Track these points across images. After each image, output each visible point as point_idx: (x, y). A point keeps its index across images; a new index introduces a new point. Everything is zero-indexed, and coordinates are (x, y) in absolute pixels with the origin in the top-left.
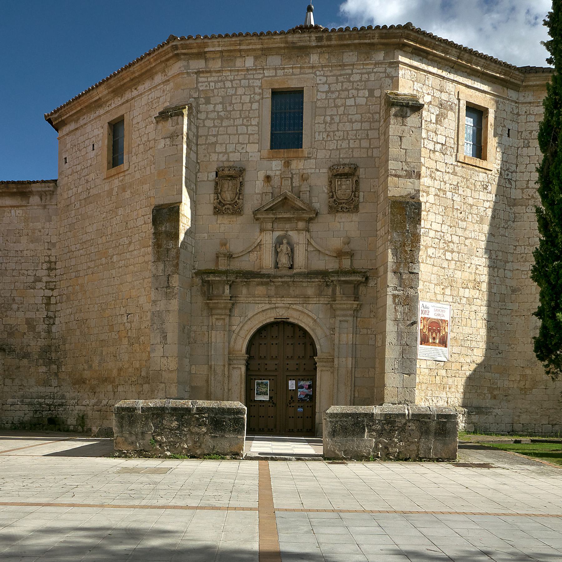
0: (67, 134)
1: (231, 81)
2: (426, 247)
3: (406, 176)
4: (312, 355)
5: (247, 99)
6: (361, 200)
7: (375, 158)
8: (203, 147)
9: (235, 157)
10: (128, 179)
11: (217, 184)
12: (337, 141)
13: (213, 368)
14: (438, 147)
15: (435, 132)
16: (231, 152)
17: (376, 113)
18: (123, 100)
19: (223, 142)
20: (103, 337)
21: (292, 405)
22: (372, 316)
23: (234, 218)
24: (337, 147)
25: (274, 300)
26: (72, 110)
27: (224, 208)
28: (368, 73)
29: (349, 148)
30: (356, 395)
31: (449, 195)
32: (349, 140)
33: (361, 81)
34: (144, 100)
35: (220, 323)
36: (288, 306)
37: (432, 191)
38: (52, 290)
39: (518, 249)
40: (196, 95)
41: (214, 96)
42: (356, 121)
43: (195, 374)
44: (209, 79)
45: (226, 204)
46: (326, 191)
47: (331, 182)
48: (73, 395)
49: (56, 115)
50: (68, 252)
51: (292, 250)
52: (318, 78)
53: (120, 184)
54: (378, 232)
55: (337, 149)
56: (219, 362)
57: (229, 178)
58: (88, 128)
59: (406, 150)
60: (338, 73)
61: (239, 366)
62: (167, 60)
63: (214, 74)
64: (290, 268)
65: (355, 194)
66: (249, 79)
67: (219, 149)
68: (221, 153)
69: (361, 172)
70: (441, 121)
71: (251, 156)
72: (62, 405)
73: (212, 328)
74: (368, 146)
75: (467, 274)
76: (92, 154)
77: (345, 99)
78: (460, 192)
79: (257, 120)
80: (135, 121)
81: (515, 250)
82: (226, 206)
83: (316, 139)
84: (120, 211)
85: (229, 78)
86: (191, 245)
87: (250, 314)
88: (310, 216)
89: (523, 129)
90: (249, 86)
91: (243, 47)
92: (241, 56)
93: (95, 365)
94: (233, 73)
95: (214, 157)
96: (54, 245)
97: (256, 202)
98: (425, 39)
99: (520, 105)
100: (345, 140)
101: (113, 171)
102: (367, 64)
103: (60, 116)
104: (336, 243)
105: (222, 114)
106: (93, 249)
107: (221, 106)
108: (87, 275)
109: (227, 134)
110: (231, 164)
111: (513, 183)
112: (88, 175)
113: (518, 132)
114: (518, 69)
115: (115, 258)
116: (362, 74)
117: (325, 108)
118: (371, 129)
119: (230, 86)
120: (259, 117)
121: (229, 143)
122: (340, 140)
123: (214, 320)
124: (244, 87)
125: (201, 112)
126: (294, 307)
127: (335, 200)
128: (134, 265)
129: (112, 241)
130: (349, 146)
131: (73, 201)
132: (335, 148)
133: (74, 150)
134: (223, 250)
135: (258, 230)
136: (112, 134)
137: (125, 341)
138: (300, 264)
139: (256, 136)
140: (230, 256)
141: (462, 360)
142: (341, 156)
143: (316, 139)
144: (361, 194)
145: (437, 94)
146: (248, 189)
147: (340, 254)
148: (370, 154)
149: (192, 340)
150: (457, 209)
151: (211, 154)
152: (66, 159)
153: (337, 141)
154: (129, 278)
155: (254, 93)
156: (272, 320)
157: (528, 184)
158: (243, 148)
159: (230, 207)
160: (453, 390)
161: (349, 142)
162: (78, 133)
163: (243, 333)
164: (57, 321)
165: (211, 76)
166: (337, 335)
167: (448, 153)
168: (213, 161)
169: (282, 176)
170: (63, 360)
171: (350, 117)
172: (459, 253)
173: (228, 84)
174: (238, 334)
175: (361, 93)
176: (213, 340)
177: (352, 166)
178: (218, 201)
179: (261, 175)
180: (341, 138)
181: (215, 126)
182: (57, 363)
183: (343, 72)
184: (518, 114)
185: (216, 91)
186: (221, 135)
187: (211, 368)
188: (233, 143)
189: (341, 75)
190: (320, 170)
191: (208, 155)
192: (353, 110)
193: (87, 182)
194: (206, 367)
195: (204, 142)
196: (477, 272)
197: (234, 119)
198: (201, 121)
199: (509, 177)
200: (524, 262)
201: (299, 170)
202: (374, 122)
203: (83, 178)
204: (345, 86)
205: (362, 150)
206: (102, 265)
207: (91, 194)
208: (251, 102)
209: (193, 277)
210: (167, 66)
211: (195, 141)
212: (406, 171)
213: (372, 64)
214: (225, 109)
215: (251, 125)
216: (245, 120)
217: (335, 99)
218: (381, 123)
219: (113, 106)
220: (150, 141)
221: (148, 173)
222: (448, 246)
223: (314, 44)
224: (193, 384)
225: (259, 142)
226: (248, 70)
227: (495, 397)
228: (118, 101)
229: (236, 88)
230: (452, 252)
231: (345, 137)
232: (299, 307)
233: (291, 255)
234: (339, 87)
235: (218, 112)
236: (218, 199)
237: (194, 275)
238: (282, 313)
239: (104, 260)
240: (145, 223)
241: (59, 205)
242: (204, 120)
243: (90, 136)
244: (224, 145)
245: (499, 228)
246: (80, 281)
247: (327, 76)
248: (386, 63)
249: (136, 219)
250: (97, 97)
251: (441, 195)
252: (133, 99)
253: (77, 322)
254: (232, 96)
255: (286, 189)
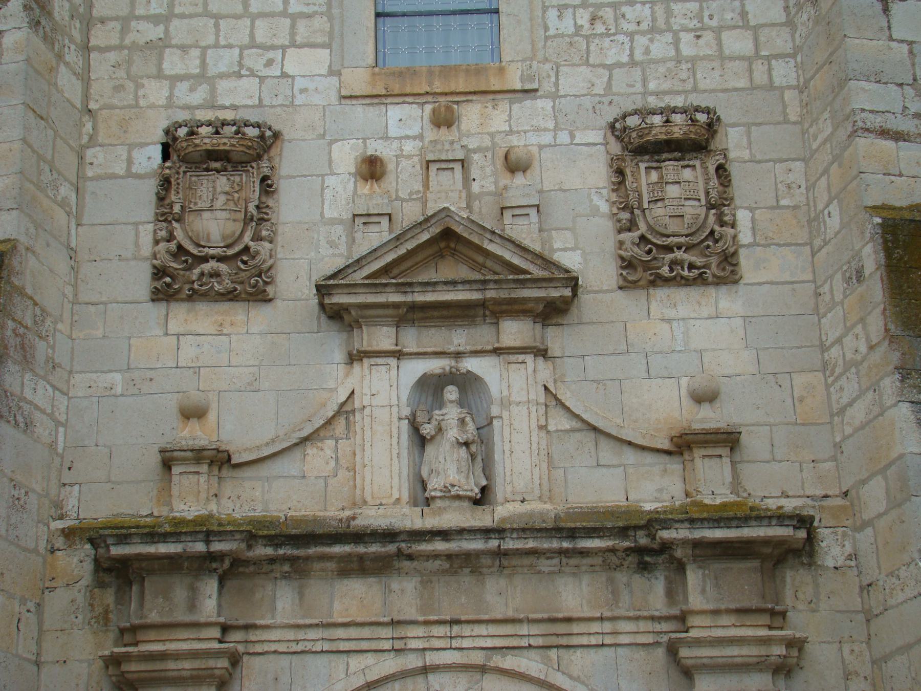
6: (745, 237)
7: (782, 89)
8: (112, 57)
11: (166, 183)
12: (631, 35)
16: (222, 76)
19: (189, 41)
23: (237, 313)
24: (631, 55)
25: (415, 636)
27: (197, 271)
32: (676, 34)
36: (477, 658)
46: (604, 207)
47: (620, 172)
57: (217, 165)
59: (910, 43)
67: (173, 63)
71: (303, 91)
83: (552, 32)
86: (51, 416)
100: (661, 32)
104: (662, 406)
109: (207, 14)
121: (216, 46)
122: (643, 33)
127: (642, 238)
130: (677, 50)
132: (625, 59)
135: (339, 356)
138: (520, 484)
140: (220, 461)
142: (652, 86)
143: (552, 32)
144: (743, 217)
146: (291, 207)
147: (684, 445)
151: (145, 81)
153: (631, 35)
168: (152, 106)
169: (430, 157)
178: (173, 246)
179: (346, 157)
180: (644, 26)
186: (182, 16)
188: (230, 46)
190: (572, 136)
191: (130, 85)
195: (115, 41)
201: (492, 135)
205: (729, 65)
209: (53, 551)
211: (76, 35)
225: (331, 42)
233: (479, 448)
236: (170, 238)
237: (60, 542)
244: (195, 53)
255: (447, 195)
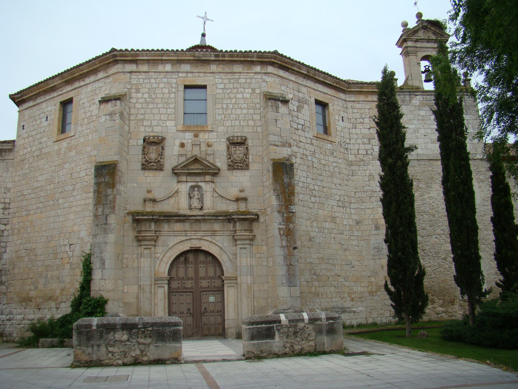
0: (26, 109)
1: (155, 79)
2: (298, 194)
3: (282, 145)
4: (220, 275)
5: (166, 91)
6: (251, 161)
8: (134, 122)
9: (158, 129)
10: (73, 142)
11: (144, 147)
12: (232, 120)
13: (142, 287)
14: (300, 127)
15: (297, 117)
16: (154, 126)
17: (258, 104)
18: (72, 88)
20: (48, 263)
21: (206, 314)
22: (264, 244)
23: (157, 173)
25: (189, 233)
26: (32, 92)
28: (251, 79)
29: (240, 126)
30: (256, 304)
31: (310, 158)
33: (246, 83)
34: (90, 88)
35: (147, 251)
36: (200, 237)
37: (299, 155)
38: (6, 225)
39: (357, 194)
40: (129, 87)
41: (142, 88)
42: (244, 108)
43: (127, 292)
44: (139, 77)
45: (151, 162)
47: (228, 148)
48: (19, 311)
49: (19, 96)
50: (21, 196)
51: (202, 196)
52: (217, 80)
53: (67, 146)
54: (264, 184)
55: (232, 126)
56: (146, 282)
58: (44, 105)
60: (230, 77)
61: (163, 285)
62: (109, 63)
63: (143, 74)
64: (200, 209)
65: (246, 157)
66: (168, 78)
67: (145, 123)
68: (147, 126)
69: (249, 142)
70: (300, 110)
72: (10, 320)
73: (142, 255)
74: (253, 124)
75: (326, 212)
76: (45, 124)
77: (236, 94)
78: (317, 156)
79: (174, 105)
80: (81, 102)
81: (355, 194)
82: (152, 164)
84: (67, 166)
85: (154, 77)
87: (171, 244)
88: (214, 172)
89: (351, 117)
90: (168, 83)
91: (163, 58)
92: (162, 63)
93: (40, 286)
94: (156, 74)
95: (142, 129)
96: (9, 190)
97: (173, 161)
98: (286, 60)
99: (347, 103)
101: (62, 136)
102: (250, 73)
103: (21, 96)
104: (234, 192)
105: (148, 100)
106: (42, 194)
107: (147, 95)
108: (37, 213)
109: (152, 113)
110: (155, 134)
111: (349, 151)
112: (41, 138)
113: (349, 119)
114: (345, 81)
115: (61, 201)
116: (246, 79)
117: (222, 99)
118: (254, 114)
119: (154, 82)
120: (175, 103)
123: (142, 250)
124: (165, 83)
125: (133, 98)
126: (205, 238)
128: (77, 206)
129: (59, 188)
131: (27, 157)
133: (31, 120)
134: (149, 196)
135: (176, 181)
136: (62, 110)
137: (68, 266)
139: (173, 116)
140: (154, 201)
141: (329, 274)
144: (250, 157)
145: (296, 93)
146: (167, 152)
148: (255, 130)
149: (124, 265)
150: (316, 168)
152: (23, 126)
153: (232, 120)
154: (72, 216)
155: (172, 87)
156: (189, 248)
157: (358, 152)
158: (164, 123)
159: (155, 164)
160: (324, 296)
161: (240, 122)
162: (35, 108)
163: (165, 259)
164: (8, 250)
165: (140, 75)
166: (238, 259)
167: (306, 130)
170: (11, 282)
171: (240, 105)
172: (320, 197)
173: (153, 81)
174: (161, 260)
175: (247, 91)
176: (142, 265)
177: (243, 138)
179: (178, 142)
181: (142, 108)
182: (6, 284)
183: (233, 77)
184: (347, 108)
185: (144, 85)
186: (147, 114)
187: (140, 287)
189: (232, 79)
192: (241, 101)
193: (40, 143)
194: (136, 287)
196: (333, 210)
197: (157, 104)
198: (132, 104)
199: (346, 147)
200: (362, 203)
202: (256, 109)
203: (37, 141)
204: (235, 86)
206: (49, 206)
207: (43, 152)
208: (169, 93)
210: (108, 67)
212: (281, 142)
213: (253, 73)
214: (150, 97)
215: (169, 108)
216: (165, 105)
217: (229, 94)
218: (262, 110)
219: (65, 91)
220: (92, 116)
221: (90, 138)
222: (312, 193)
223: (213, 58)
224: (125, 301)
226: (167, 72)
227: (352, 300)
228: (69, 88)
229: (158, 83)
230: (315, 197)
231: (237, 118)
232: (208, 238)
233: (201, 199)
234: (231, 86)
235: (145, 99)
236: (145, 158)
237: (126, 215)
238: (195, 244)
239: (51, 203)
240: (87, 175)
241: (15, 160)
242: (135, 104)
243: (45, 111)
244: (149, 121)
245: (343, 180)
246: (30, 218)
247: (222, 79)
248: (262, 73)
249: (79, 172)
250: (53, 85)
251: (305, 158)
252: (80, 87)
253: (26, 251)
254: (155, 88)
255: (196, 152)
